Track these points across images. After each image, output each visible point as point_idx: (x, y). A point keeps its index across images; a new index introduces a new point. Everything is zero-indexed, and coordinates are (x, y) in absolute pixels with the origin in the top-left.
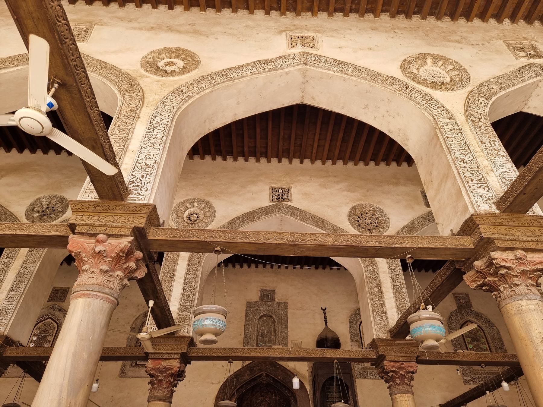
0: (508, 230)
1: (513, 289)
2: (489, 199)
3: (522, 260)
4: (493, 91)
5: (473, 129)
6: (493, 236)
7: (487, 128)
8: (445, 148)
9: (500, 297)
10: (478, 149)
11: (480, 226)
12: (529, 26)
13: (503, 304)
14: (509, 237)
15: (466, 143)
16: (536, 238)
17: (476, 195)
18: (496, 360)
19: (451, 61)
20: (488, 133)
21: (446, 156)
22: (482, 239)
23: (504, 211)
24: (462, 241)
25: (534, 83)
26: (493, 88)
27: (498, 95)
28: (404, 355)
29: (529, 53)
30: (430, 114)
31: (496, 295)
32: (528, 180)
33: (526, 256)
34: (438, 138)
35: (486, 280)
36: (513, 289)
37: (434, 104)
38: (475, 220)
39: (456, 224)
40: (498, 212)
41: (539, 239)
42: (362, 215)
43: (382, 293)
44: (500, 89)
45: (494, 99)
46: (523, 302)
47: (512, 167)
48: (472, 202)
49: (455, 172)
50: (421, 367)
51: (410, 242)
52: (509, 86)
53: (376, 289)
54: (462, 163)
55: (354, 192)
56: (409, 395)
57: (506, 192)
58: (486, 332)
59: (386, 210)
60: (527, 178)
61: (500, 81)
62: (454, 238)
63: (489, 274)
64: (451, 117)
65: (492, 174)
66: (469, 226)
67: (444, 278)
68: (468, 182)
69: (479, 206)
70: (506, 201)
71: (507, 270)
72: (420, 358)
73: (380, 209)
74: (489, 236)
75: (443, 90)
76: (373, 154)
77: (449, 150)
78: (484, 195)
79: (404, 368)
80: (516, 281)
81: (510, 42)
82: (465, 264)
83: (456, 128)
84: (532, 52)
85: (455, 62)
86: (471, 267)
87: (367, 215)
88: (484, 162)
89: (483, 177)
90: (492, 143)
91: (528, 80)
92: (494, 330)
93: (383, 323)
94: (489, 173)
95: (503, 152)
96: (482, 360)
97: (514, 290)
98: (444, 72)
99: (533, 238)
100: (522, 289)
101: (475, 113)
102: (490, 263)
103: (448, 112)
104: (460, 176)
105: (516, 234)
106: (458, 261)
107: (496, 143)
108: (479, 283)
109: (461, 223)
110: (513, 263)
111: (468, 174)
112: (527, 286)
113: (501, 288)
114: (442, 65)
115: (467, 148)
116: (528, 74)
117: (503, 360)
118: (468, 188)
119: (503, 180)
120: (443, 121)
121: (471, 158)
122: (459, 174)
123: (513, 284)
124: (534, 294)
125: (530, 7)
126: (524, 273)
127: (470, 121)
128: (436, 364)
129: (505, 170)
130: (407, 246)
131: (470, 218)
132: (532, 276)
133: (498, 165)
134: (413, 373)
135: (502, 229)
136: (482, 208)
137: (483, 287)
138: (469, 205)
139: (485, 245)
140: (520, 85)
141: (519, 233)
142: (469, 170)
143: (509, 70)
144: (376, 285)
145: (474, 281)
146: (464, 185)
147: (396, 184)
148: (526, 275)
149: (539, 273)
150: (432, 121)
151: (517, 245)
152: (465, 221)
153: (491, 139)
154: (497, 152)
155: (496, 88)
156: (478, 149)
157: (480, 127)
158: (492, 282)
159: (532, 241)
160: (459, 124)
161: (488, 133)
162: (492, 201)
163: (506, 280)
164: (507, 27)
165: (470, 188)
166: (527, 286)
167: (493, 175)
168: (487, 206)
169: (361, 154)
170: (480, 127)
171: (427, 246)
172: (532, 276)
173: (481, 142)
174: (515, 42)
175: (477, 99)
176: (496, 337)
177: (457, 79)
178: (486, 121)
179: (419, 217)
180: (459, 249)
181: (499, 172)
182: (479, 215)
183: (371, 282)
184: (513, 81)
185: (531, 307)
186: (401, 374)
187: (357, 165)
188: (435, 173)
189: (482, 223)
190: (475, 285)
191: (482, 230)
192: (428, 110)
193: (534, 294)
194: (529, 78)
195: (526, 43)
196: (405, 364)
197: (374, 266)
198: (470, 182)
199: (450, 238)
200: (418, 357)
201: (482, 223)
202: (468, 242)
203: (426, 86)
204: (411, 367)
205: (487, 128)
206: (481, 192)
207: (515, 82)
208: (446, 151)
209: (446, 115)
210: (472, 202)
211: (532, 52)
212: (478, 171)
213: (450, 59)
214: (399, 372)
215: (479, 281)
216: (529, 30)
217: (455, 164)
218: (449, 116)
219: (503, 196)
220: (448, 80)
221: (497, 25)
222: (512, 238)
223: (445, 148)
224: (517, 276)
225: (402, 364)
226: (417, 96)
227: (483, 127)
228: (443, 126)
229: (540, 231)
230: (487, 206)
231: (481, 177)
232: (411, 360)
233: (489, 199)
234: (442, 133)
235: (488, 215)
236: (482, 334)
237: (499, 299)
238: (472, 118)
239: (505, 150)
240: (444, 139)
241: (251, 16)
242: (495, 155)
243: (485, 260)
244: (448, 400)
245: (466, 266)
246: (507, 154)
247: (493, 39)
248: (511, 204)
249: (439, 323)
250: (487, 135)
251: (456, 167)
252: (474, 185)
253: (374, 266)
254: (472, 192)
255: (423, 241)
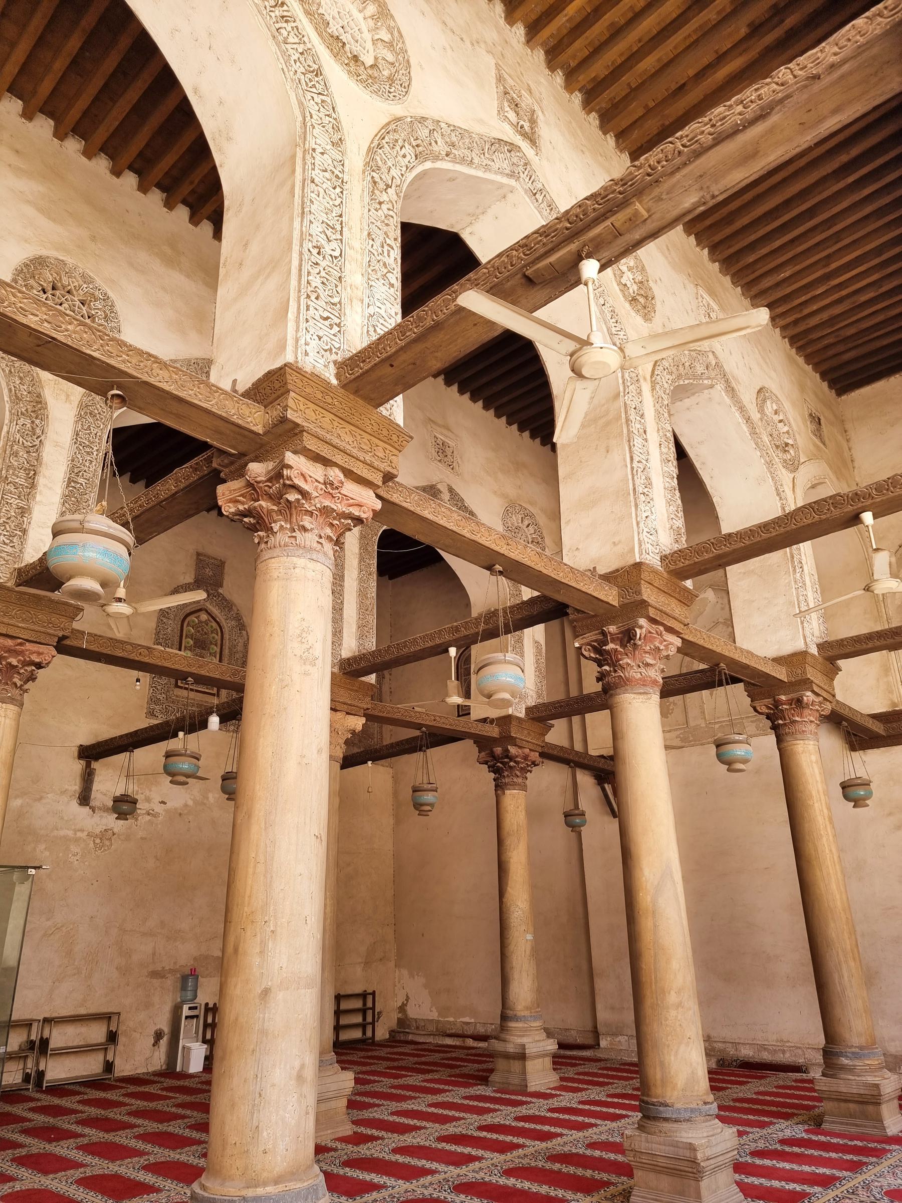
0: (336, 424)
1: (294, 534)
2: (331, 350)
3: (333, 489)
4: (435, 148)
5: (367, 199)
6: (304, 424)
7: (391, 213)
8: (297, 199)
9: (267, 542)
10: (357, 245)
11: (292, 394)
12: (547, 72)
13: (266, 555)
14: (332, 438)
15: (341, 216)
16: (373, 460)
17: (312, 331)
18: (217, 677)
19: (392, 24)
20: (387, 225)
21: (292, 220)
22: (284, 420)
23: (344, 386)
24: (245, 411)
25: (501, 186)
26: (436, 142)
27: (439, 165)
28: (36, 628)
29: (522, 123)
30: (301, 104)
31: (261, 538)
32: (408, 340)
33: (342, 483)
34: (294, 171)
35: (256, 504)
36: (294, 534)
37: (320, 87)
38: (288, 376)
39: (248, 374)
40: (335, 382)
41: (376, 464)
42: (54, 288)
43: (33, 486)
44: (447, 155)
45: (428, 165)
46: (301, 562)
47: (396, 314)
48: (297, 340)
49: (295, 263)
50: (61, 660)
51: (134, 361)
52: (463, 161)
53: (22, 474)
54: (315, 251)
55: (54, 220)
56: (11, 707)
57: (365, 349)
58: (226, 636)
59: (120, 307)
60: (408, 334)
61: (454, 139)
62: (232, 397)
63: (267, 494)
64: (338, 143)
65: (357, 306)
66: (272, 387)
67: (182, 486)
68: (308, 297)
69: (306, 354)
70: (358, 366)
71: (300, 497)
72: (67, 642)
73: (106, 298)
74: (299, 421)
75: (349, 72)
76: (141, 154)
77: (303, 208)
78: (325, 338)
79: (22, 653)
80: (307, 522)
81: (506, 76)
82: (232, 463)
83: (336, 172)
84: (527, 126)
85: (399, 32)
86: (240, 472)
87: (68, 296)
88: (355, 277)
89: (340, 303)
90: (386, 247)
91: (496, 173)
92: (241, 635)
93: (8, 549)
94: (355, 302)
95: (396, 277)
96: (193, 670)
97: (295, 537)
98: (367, 36)
99: (368, 458)
100: (310, 539)
101: (384, 169)
102: (277, 475)
103: (337, 128)
104: (300, 276)
105: (345, 437)
106: (222, 452)
107: (392, 251)
108: (241, 507)
109: (260, 374)
110: (316, 488)
111: (316, 282)
112: (321, 537)
113: (276, 527)
114: (372, 17)
115: (338, 227)
116: (501, 161)
117: (229, 679)
118: (303, 307)
119: (371, 329)
120: (320, 139)
121: (337, 254)
122: (300, 270)
123: (299, 526)
124: (325, 554)
125: (565, 31)
126: (325, 511)
127: (369, 178)
128: (99, 661)
129: (382, 312)
130: (122, 367)
131: (281, 369)
132: (335, 522)
133: (377, 296)
134: (39, 666)
135: (327, 420)
136: (310, 359)
137: (246, 516)
138: (290, 342)
139: (286, 433)
140: (480, 174)
141: (350, 439)
142: (323, 274)
143: (477, 129)
144: (26, 465)
145: (236, 501)
146: (299, 297)
147: (170, 262)
148: (327, 517)
149: (350, 521)
150: (298, 124)
151: (338, 458)
152: (269, 372)
153: (388, 241)
154: (386, 271)
155: (441, 147)
156: (357, 245)
157: (380, 203)
158: (265, 511)
159: (364, 462)
160: (346, 170)
161: (387, 225)
162: (334, 357)
163: (291, 515)
164: (514, 42)
165: (308, 309)
166: (321, 537)
167: (359, 310)
168: (322, 361)
169: (112, 135)
170: (380, 203)
171: (167, 388)
172: (335, 522)
173: (369, 234)
174: (513, 83)
175: (400, 143)
176: (240, 648)
177: (386, 73)
178: (395, 197)
179: (189, 361)
180: (233, 424)
181: (371, 310)
182: (299, 371)
183: (16, 454)
184: (474, 155)
185: (310, 574)
186: (10, 664)
187: (89, 158)
188: (254, 248)
189: (297, 390)
190: (232, 510)
191: (291, 403)
192: (301, 92)
193: (325, 554)
194: (499, 171)
195: (527, 101)
196: (28, 646)
197: (37, 422)
198: (313, 298)
199: (225, 392)
200: (64, 638)
201: (297, 390)
202: (255, 419)
203: (320, 35)
204: (39, 654)
205: (391, 213)
206: (323, 329)
207: (476, 161)
208: (297, 210)
209: (331, 130)
210: (297, 340)
211: (527, 126)
212: (336, 286)
213: (392, 16)
214: (5, 658)
215: (243, 503)
216: (543, 80)
217: (301, 246)
218: (336, 138)
219: (356, 355)
220: (369, 61)
221: (502, 21)
222: (335, 441)
223: (297, 199)
224: (311, 514)
225: (21, 644)
226: (291, 40)
227: (384, 207)
228: (314, 150)
229: (384, 449)
230: (322, 361)
231: (336, 300)
232: (47, 640)
233: (331, 350)
234: (305, 164)
235: (315, 379)
236: (218, 638)
237: (263, 546)
238: (374, 174)
239: (399, 276)
240: (304, 180)
241: (140, 195)
242: (379, 274)
243: (271, 465)
244: (100, 739)
245: (232, 468)
246: (400, 284)
247: (483, 46)
248: (362, 375)
249: (123, 551)
250: (385, 228)
251: (301, 254)
252: (319, 308)
253: (37, 422)
254: (307, 321)
255: (164, 374)
